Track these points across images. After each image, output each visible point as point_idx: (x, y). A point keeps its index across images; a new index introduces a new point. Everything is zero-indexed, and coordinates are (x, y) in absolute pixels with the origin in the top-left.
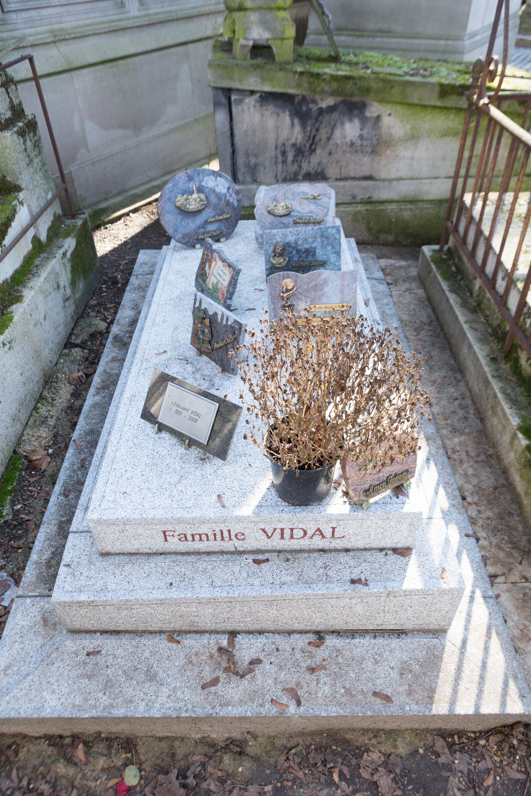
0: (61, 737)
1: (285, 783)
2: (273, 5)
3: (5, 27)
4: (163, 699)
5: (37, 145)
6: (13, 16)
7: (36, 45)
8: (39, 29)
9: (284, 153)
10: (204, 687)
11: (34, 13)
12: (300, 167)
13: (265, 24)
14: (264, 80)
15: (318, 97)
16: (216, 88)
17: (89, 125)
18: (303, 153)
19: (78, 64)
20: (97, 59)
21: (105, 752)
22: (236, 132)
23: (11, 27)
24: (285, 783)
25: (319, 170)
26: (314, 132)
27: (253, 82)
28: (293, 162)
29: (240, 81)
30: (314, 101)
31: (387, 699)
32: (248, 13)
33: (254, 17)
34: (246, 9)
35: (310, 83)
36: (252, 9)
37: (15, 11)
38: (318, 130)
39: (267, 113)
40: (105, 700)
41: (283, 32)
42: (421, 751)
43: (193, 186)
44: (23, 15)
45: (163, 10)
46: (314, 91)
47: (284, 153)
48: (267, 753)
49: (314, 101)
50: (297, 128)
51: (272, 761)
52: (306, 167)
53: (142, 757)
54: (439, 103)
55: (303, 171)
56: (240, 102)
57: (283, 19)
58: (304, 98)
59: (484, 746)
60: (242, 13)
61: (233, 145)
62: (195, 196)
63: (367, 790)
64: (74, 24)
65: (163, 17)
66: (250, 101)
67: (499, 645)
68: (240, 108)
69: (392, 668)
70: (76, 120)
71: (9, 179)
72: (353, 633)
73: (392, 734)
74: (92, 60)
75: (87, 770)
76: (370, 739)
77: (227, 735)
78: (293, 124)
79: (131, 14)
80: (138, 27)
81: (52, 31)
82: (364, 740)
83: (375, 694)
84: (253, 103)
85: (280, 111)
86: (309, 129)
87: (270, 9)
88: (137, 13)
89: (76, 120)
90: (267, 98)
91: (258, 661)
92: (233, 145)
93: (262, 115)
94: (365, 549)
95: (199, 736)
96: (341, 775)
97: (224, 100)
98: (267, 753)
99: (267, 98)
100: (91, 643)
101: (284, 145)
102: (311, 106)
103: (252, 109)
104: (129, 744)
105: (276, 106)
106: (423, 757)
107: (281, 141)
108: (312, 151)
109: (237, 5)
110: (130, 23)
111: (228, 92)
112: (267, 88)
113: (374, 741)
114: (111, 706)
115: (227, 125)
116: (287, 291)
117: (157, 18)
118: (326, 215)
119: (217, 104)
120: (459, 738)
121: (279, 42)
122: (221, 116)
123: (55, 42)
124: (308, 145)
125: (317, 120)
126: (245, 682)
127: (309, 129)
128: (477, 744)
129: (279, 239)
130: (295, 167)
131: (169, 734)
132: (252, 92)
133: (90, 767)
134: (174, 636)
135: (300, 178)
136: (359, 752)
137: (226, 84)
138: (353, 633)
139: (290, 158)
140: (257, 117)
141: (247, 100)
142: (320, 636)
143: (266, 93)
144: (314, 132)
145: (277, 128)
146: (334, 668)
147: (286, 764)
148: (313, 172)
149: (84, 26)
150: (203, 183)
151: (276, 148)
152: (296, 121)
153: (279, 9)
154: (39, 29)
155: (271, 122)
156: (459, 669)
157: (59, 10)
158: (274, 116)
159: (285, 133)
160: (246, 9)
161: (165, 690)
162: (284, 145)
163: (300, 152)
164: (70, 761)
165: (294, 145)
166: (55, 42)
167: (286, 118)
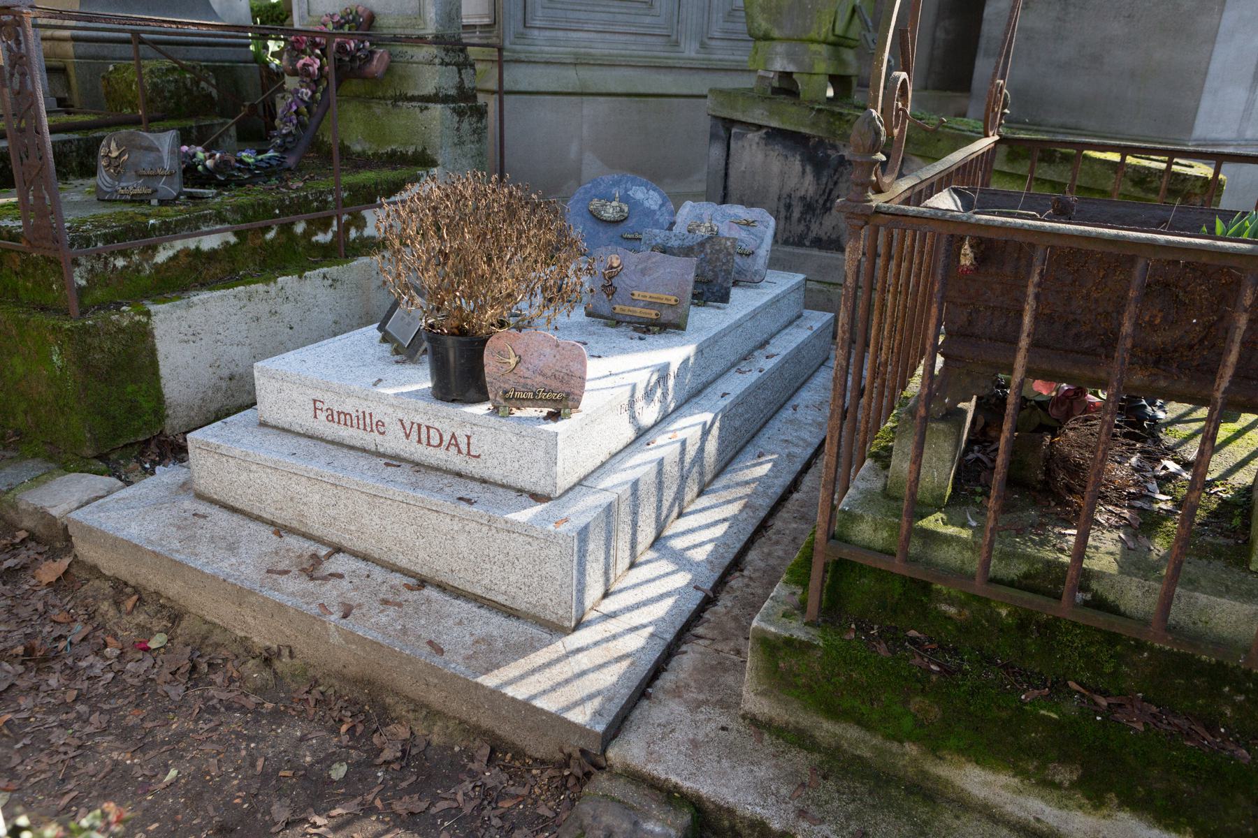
0: (126, 584)
1: (290, 710)
2: (804, 37)
3: (522, 41)
4: (226, 564)
5: (479, 133)
6: (536, 32)
7: (552, 63)
8: (561, 49)
9: (789, 207)
10: (268, 572)
11: (560, 34)
12: (808, 228)
13: (791, 57)
14: (772, 113)
15: (839, 143)
16: (715, 117)
17: (589, 157)
18: (814, 210)
19: (594, 90)
20: (620, 90)
21: (152, 614)
22: (732, 172)
23: (529, 41)
24: (290, 710)
25: (834, 236)
26: (830, 186)
27: (758, 115)
28: (799, 221)
29: (744, 112)
30: (834, 147)
31: (440, 651)
32: (774, 43)
33: (780, 48)
34: (773, 39)
35: (829, 123)
36: (779, 39)
37: (539, 28)
38: (836, 183)
39: (773, 154)
40: (176, 545)
41: (812, 66)
42: (457, 749)
43: (617, 192)
44: (548, 33)
45: (732, 58)
46: (834, 134)
47: (789, 207)
48: (293, 675)
49: (834, 147)
50: (809, 177)
51: (294, 686)
52: (815, 230)
53: (179, 631)
54: (1006, 169)
55: (812, 235)
56: (741, 136)
57: (815, 53)
58: (821, 141)
59: (534, 776)
60: (767, 43)
61: (725, 188)
62: (614, 204)
63: (366, 751)
64: (606, 52)
65: (727, 65)
66: (754, 137)
67: (621, 671)
68: (740, 143)
69: (472, 635)
70: (574, 148)
71: (429, 152)
72: (458, 594)
73: (433, 714)
74: (613, 90)
75: (126, 619)
76: (408, 712)
77: (268, 643)
78: (804, 172)
79: (686, 54)
80: (691, 69)
81: (575, 54)
82: (401, 710)
83: (430, 643)
84: (757, 139)
85: (789, 154)
86: (824, 180)
87: (801, 40)
88: (693, 55)
89: (574, 148)
90: (775, 135)
91: (341, 576)
92: (725, 188)
93: (766, 156)
94: (503, 486)
95: (243, 634)
96: (351, 730)
97: (722, 133)
98: (293, 675)
99: (775, 135)
100: (203, 508)
101: (790, 196)
102: (829, 152)
103: (754, 147)
104: (176, 617)
105: (785, 147)
106: (455, 755)
107: (786, 190)
108: (827, 209)
109: (761, 33)
110: (681, 63)
111: (729, 123)
112: (774, 124)
113: (411, 716)
114: (177, 551)
115: (723, 163)
116: (612, 268)
117: (720, 65)
118: (759, 247)
119: (714, 136)
120: (513, 758)
121: (806, 77)
122: (717, 151)
123: (575, 64)
124: (821, 202)
125: (836, 171)
126: (311, 584)
127: (824, 180)
128: (529, 771)
129: (659, 241)
130: (802, 227)
131: (217, 621)
132: (760, 127)
133: (129, 618)
134: (280, 529)
135: (807, 243)
136: (385, 716)
137: (726, 113)
138: (458, 594)
139: (796, 214)
140: (760, 157)
141: (750, 136)
142: (423, 583)
143: (774, 129)
144: (830, 186)
145: (782, 173)
146: (410, 610)
147: (305, 696)
148: (825, 238)
149: (617, 56)
150: (630, 193)
151: (779, 199)
152: (808, 169)
153: (813, 41)
154: (561, 49)
155: (776, 165)
156: (549, 664)
157: (592, 35)
158: (781, 158)
159: (792, 182)
160: (773, 39)
161: (233, 560)
162: (790, 196)
163: (809, 208)
164: (117, 604)
165: (803, 198)
166: (575, 64)
167: (796, 164)
